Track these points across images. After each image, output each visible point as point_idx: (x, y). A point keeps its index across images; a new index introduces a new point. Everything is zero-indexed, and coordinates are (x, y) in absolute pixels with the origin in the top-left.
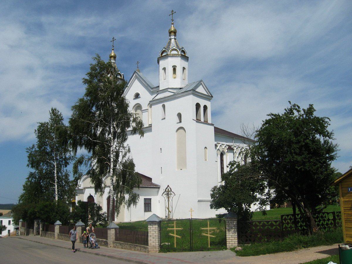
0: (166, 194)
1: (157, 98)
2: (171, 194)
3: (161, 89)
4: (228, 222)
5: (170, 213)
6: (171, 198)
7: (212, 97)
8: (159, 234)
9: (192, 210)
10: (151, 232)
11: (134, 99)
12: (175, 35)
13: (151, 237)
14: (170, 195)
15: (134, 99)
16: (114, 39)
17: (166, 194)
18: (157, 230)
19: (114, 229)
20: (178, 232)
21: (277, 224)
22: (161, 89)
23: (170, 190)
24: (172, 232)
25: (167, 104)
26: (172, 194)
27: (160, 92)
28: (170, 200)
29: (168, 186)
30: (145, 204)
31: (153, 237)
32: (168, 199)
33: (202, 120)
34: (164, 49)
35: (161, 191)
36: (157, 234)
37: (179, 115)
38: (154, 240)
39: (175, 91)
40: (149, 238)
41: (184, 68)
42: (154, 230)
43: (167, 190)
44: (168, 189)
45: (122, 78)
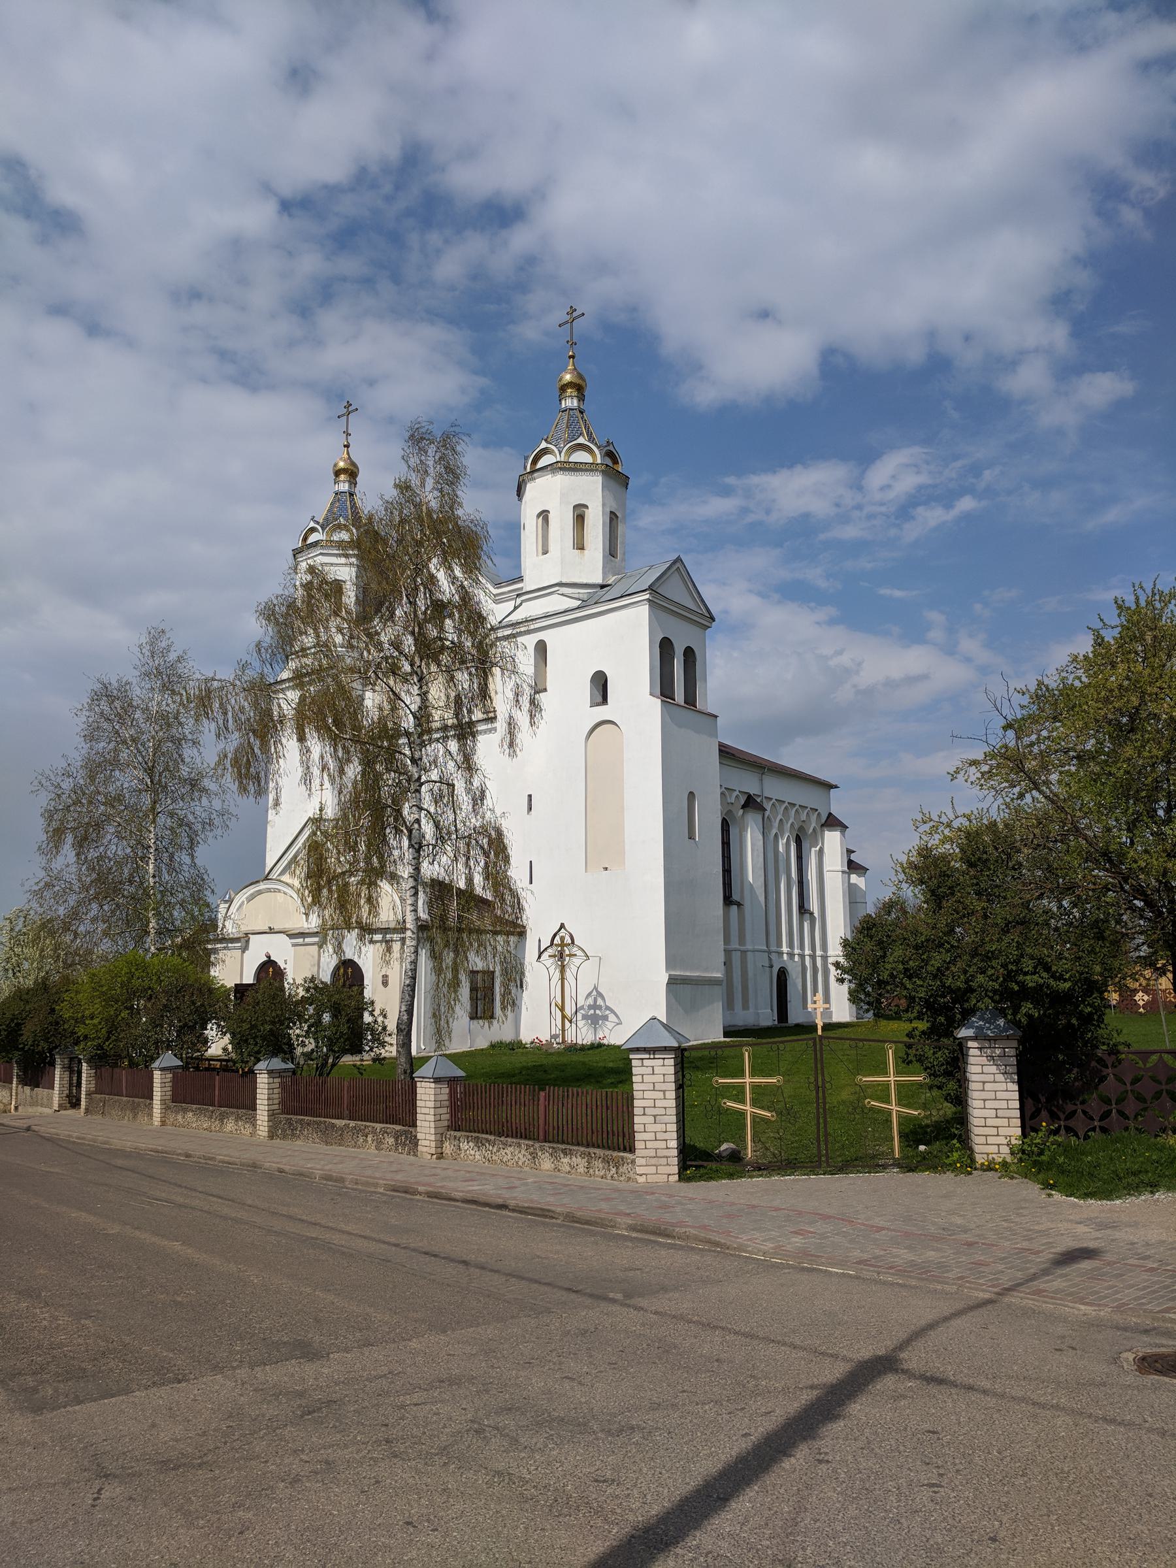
0: (554, 956)
2: (570, 955)
5: (567, 1024)
6: (574, 970)
7: (713, 619)
14: (567, 958)
16: (351, 409)
17: (554, 956)
20: (761, 1096)
23: (568, 940)
24: (738, 1094)
26: (575, 955)
28: (569, 975)
29: (562, 926)
31: (655, 1116)
32: (563, 969)
40: (637, 1119)
43: (557, 940)
44: (562, 939)
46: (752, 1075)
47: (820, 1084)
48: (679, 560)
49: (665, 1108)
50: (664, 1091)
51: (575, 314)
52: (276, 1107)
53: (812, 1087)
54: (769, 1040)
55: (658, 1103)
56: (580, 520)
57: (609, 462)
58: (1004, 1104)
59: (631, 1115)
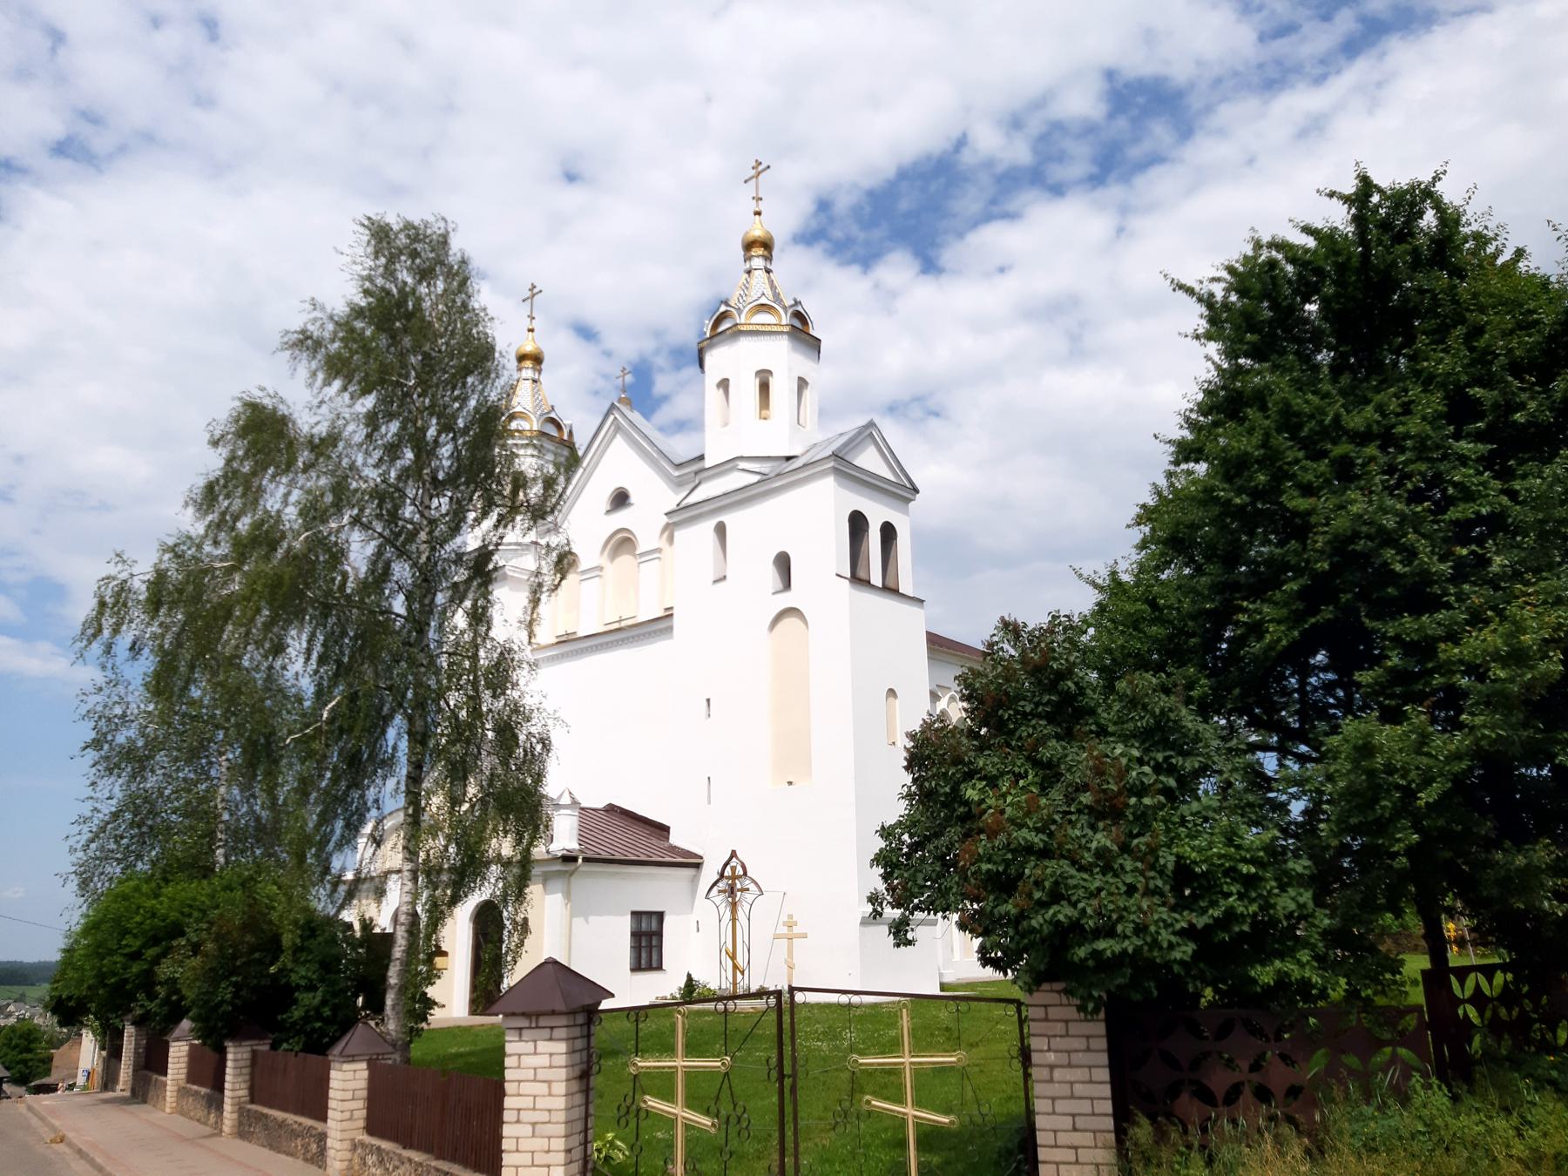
0: (724, 891)
1: (693, 499)
2: (743, 890)
3: (708, 463)
4: (1040, 1013)
5: (739, 975)
7: (916, 491)
8: (579, 1099)
9: (796, 930)
10: (527, 1088)
11: (608, 512)
12: (768, 258)
13: (518, 1121)
14: (739, 894)
15: (608, 512)
16: (535, 291)
17: (724, 891)
18: (562, 1074)
19: (563, 1021)
21: (1388, 1050)
22: (708, 463)
23: (740, 871)
24: (663, 1085)
25: (730, 519)
27: (705, 474)
28: (741, 915)
29: (733, 854)
30: (636, 935)
31: (534, 1124)
32: (734, 906)
33: (876, 579)
34: (723, 308)
35: (709, 873)
36: (561, 1103)
37: (783, 563)
38: (540, 1143)
39: (765, 467)
40: (507, 1130)
41: (802, 383)
42: (542, 1075)
43: (728, 872)
45: (566, 437)
46: (917, 1049)
47: (787, 1070)
48: (871, 424)
49: (550, 1111)
50: (549, 1082)
51: (760, 168)
52: (241, 1093)
53: (774, 1074)
54: (856, 999)
55: (541, 1103)
56: (764, 388)
57: (798, 324)
58: (1085, 1107)
59: (498, 1122)
